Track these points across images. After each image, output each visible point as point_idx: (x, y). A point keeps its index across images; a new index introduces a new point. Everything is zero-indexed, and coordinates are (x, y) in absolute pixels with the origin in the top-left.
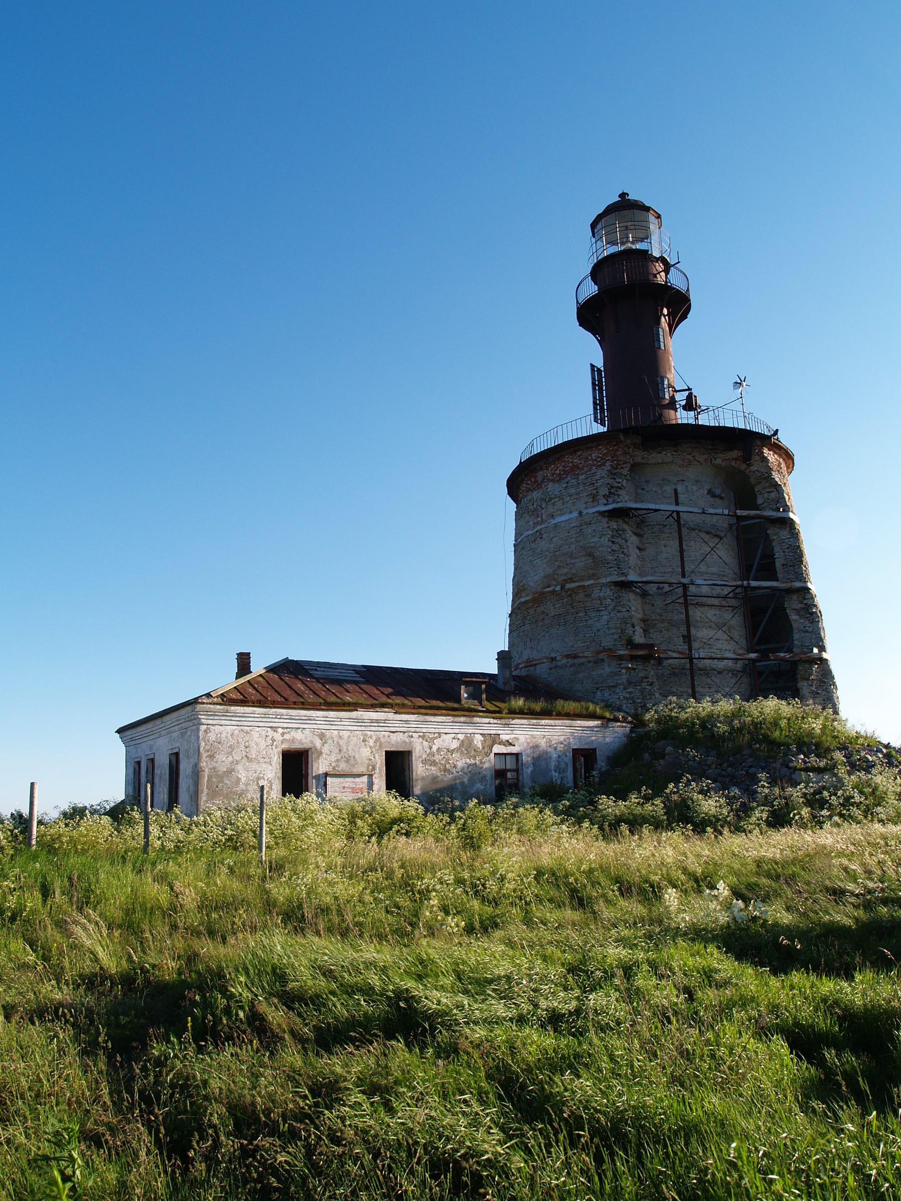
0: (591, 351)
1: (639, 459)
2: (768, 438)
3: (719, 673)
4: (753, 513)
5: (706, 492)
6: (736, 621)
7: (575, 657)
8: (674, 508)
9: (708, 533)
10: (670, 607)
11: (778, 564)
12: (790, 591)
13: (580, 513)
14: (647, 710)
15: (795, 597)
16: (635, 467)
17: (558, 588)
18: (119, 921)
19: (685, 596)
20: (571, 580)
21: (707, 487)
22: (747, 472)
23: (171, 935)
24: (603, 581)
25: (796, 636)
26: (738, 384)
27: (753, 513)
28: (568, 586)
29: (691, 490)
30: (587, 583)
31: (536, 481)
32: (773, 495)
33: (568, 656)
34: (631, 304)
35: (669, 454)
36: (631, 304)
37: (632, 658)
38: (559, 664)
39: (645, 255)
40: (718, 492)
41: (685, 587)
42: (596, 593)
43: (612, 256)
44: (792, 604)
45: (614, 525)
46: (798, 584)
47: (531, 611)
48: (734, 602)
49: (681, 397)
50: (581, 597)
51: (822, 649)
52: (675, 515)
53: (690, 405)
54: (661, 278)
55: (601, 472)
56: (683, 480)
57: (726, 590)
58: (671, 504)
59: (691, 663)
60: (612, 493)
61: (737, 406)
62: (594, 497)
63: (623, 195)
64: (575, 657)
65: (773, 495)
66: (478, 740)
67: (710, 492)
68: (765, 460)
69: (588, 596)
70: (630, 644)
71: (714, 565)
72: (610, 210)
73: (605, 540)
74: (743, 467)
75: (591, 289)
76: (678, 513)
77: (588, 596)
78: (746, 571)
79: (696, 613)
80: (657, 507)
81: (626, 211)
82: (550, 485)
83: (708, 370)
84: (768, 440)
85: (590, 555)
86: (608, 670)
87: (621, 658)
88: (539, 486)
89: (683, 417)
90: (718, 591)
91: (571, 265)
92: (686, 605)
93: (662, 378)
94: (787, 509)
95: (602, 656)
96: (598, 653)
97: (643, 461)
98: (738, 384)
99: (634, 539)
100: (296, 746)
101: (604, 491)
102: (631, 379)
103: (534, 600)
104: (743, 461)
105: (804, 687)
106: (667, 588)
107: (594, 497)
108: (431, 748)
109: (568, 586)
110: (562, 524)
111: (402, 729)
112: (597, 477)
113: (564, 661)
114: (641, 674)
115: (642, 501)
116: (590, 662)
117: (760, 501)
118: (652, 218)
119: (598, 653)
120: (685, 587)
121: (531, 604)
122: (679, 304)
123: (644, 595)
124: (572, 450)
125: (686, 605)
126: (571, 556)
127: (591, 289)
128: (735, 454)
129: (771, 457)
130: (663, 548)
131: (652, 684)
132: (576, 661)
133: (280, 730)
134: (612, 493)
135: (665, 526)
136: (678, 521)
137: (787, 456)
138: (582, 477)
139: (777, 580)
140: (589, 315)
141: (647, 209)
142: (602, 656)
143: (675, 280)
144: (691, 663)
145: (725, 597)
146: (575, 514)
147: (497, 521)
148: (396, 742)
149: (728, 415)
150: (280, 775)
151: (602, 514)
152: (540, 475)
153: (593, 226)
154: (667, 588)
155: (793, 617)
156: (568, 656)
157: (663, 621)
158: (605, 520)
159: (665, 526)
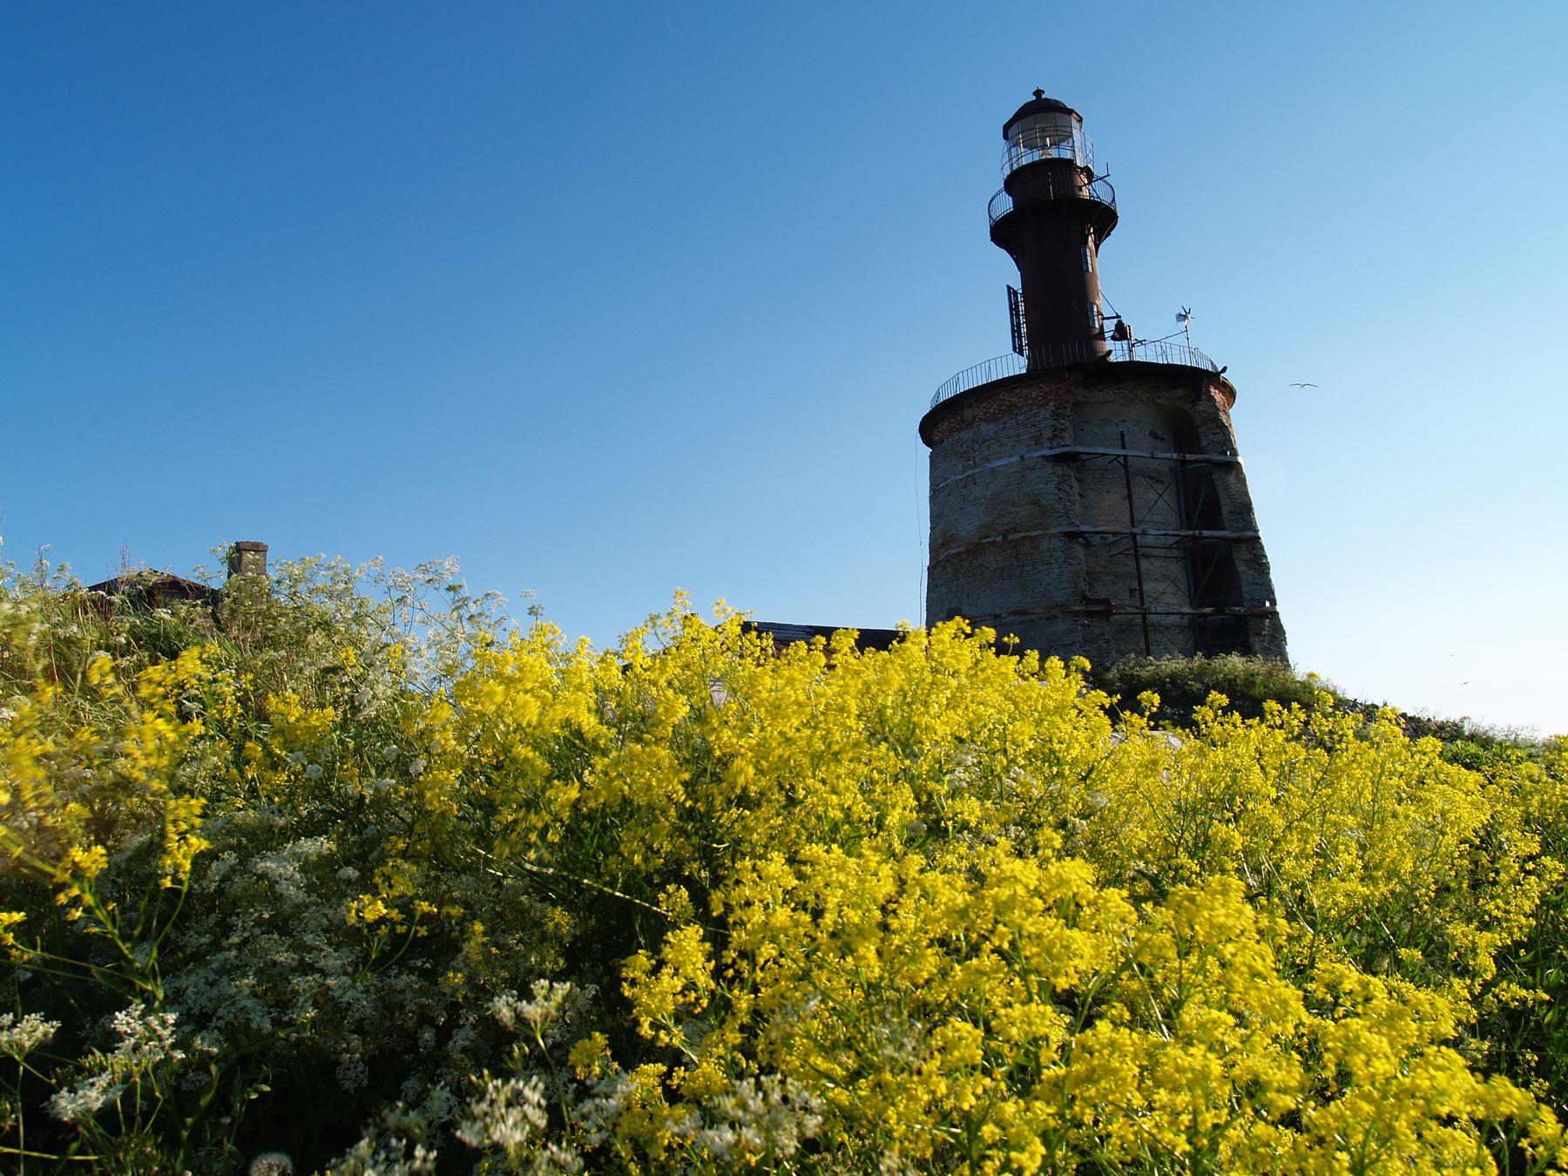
0: (1005, 271)
1: (1079, 398)
2: (1217, 374)
4: (1201, 457)
6: (1175, 569)
7: (1024, 613)
8: (1122, 452)
11: (1224, 511)
12: (1238, 541)
13: (1022, 457)
14: (1108, 670)
15: (1243, 547)
16: (1077, 405)
17: (999, 539)
18: (773, 920)
19: (1136, 547)
20: (1015, 531)
21: (1149, 428)
23: (818, 926)
24: (1053, 531)
25: (1245, 589)
26: (1182, 317)
27: (1201, 457)
28: (1011, 537)
29: (1133, 435)
30: (1034, 534)
31: (963, 421)
32: (1219, 437)
33: (1014, 613)
34: (1052, 222)
36: (1052, 222)
37: (1089, 614)
39: (1070, 163)
40: (1160, 433)
41: (1134, 535)
42: (1044, 545)
43: (1032, 165)
44: (1242, 554)
45: (1059, 470)
46: (1249, 534)
47: (966, 564)
48: (1177, 553)
49: (1110, 326)
51: (1274, 603)
52: (1121, 460)
53: (1121, 333)
54: (1085, 193)
55: (1044, 413)
57: (1172, 540)
58: (1113, 447)
59: (1144, 618)
60: (1056, 436)
61: (1181, 339)
62: (1037, 440)
63: (1038, 93)
64: (1024, 613)
65: (1219, 437)
67: (1153, 435)
68: (1212, 399)
69: (1036, 547)
70: (1084, 598)
71: (1159, 516)
72: (1025, 112)
73: (1052, 487)
74: (1188, 406)
75: (1006, 204)
76: (1125, 457)
77: (1036, 547)
78: (1187, 519)
79: (1144, 563)
80: (1101, 451)
81: (1042, 115)
82: (984, 425)
83: (1145, 300)
84: (1213, 378)
85: (1034, 503)
86: (1062, 627)
87: (1076, 614)
88: (969, 425)
89: (1117, 352)
90: (1163, 541)
91: (982, 178)
92: (1137, 556)
93: (1092, 304)
94: (1235, 453)
95: (1054, 612)
96: (1050, 609)
98: (1182, 317)
99: (1076, 485)
101: (1048, 433)
102: (1055, 303)
103: (967, 551)
104: (1187, 403)
105: (1254, 640)
106: (1111, 538)
107: (1037, 440)
109: (1011, 537)
113: (1011, 618)
114: (1097, 631)
115: (1082, 445)
117: (1204, 443)
118: (1074, 123)
119: (1050, 609)
120: (1134, 535)
122: (1104, 219)
123: (1087, 545)
125: (1137, 556)
126: (1013, 505)
127: (1006, 204)
128: (1179, 392)
129: (1218, 396)
131: (1108, 642)
132: (1025, 618)
134: (1056, 436)
136: (1125, 466)
137: (1230, 393)
138: (1021, 418)
139: (1223, 528)
140: (1002, 233)
141: (1070, 112)
142: (1054, 612)
143: (1099, 192)
144: (1144, 618)
145: (1170, 548)
146: (1016, 458)
147: (915, 462)
149: (1176, 351)
151: (1046, 458)
152: (968, 414)
153: (1007, 128)
154: (1111, 538)
155: (1242, 568)
156: (1014, 613)
158: (1049, 465)
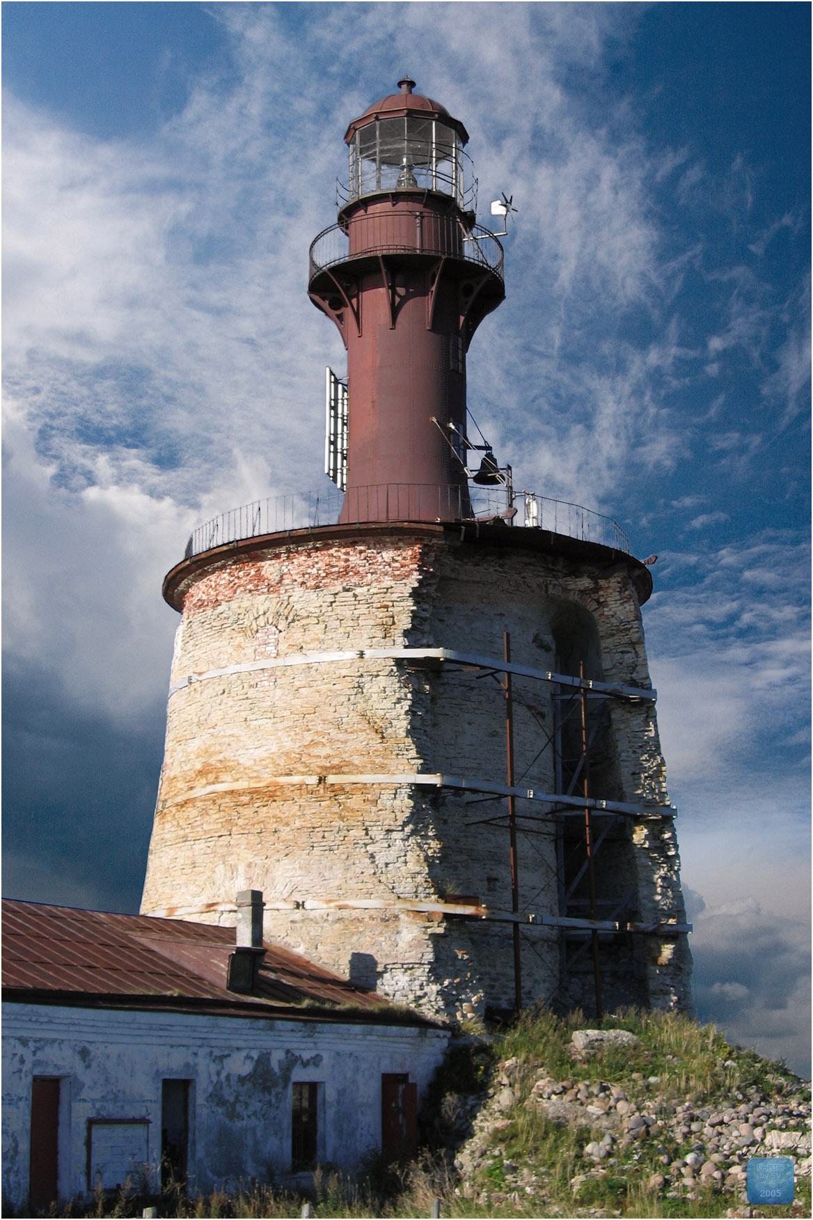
3: (533, 944)
5: (531, 638)
9: (530, 708)
10: (472, 829)
17: (313, 780)
20: (338, 769)
21: (533, 631)
22: (596, 615)
28: (331, 779)
35: (491, 570)
38: (312, 914)
50: (355, 801)
56: (502, 615)
66: (277, 1057)
97: (453, 576)
100: (51, 1071)
108: (218, 1074)
110: (322, 668)
111: (184, 1042)
112: (394, 597)
116: (372, 918)
121: (245, 799)
124: (350, 540)
130: (466, 726)
133: (31, 1044)
135: (472, 689)
146: (351, 655)
148: (175, 1062)
150: (28, 1125)
157: (461, 851)
159: (472, 689)
